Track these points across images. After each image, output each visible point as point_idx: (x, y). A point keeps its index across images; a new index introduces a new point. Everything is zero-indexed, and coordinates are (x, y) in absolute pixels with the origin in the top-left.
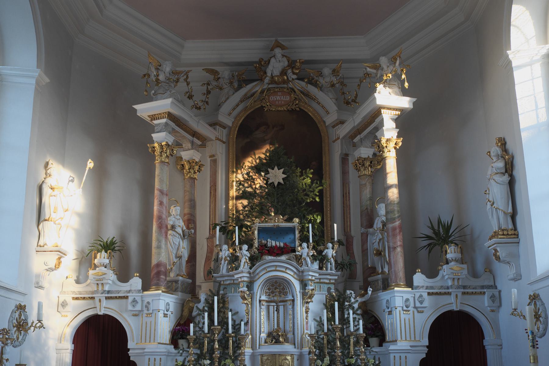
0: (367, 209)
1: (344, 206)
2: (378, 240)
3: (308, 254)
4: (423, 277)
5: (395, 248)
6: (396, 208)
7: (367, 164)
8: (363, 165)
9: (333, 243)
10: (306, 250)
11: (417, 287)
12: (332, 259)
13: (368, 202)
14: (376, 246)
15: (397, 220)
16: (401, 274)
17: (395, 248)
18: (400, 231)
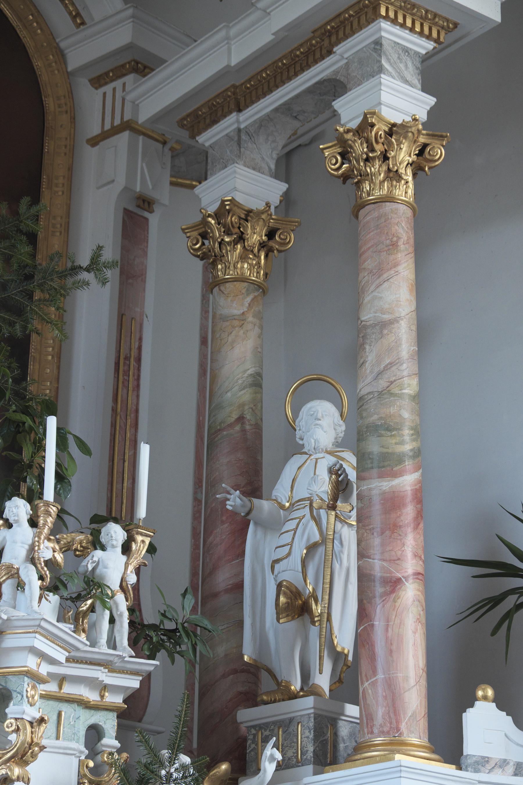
0: (241, 419)
1: (114, 410)
2: (299, 550)
3: (32, 549)
4: (504, 721)
5: (394, 584)
6: (406, 415)
7: (255, 236)
8: (241, 238)
9: (130, 526)
10: (23, 533)
11: (482, 763)
12: (120, 597)
13: (246, 396)
14: (290, 571)
15: (408, 464)
16: (414, 699)
17: (398, 581)
18: (419, 515)
